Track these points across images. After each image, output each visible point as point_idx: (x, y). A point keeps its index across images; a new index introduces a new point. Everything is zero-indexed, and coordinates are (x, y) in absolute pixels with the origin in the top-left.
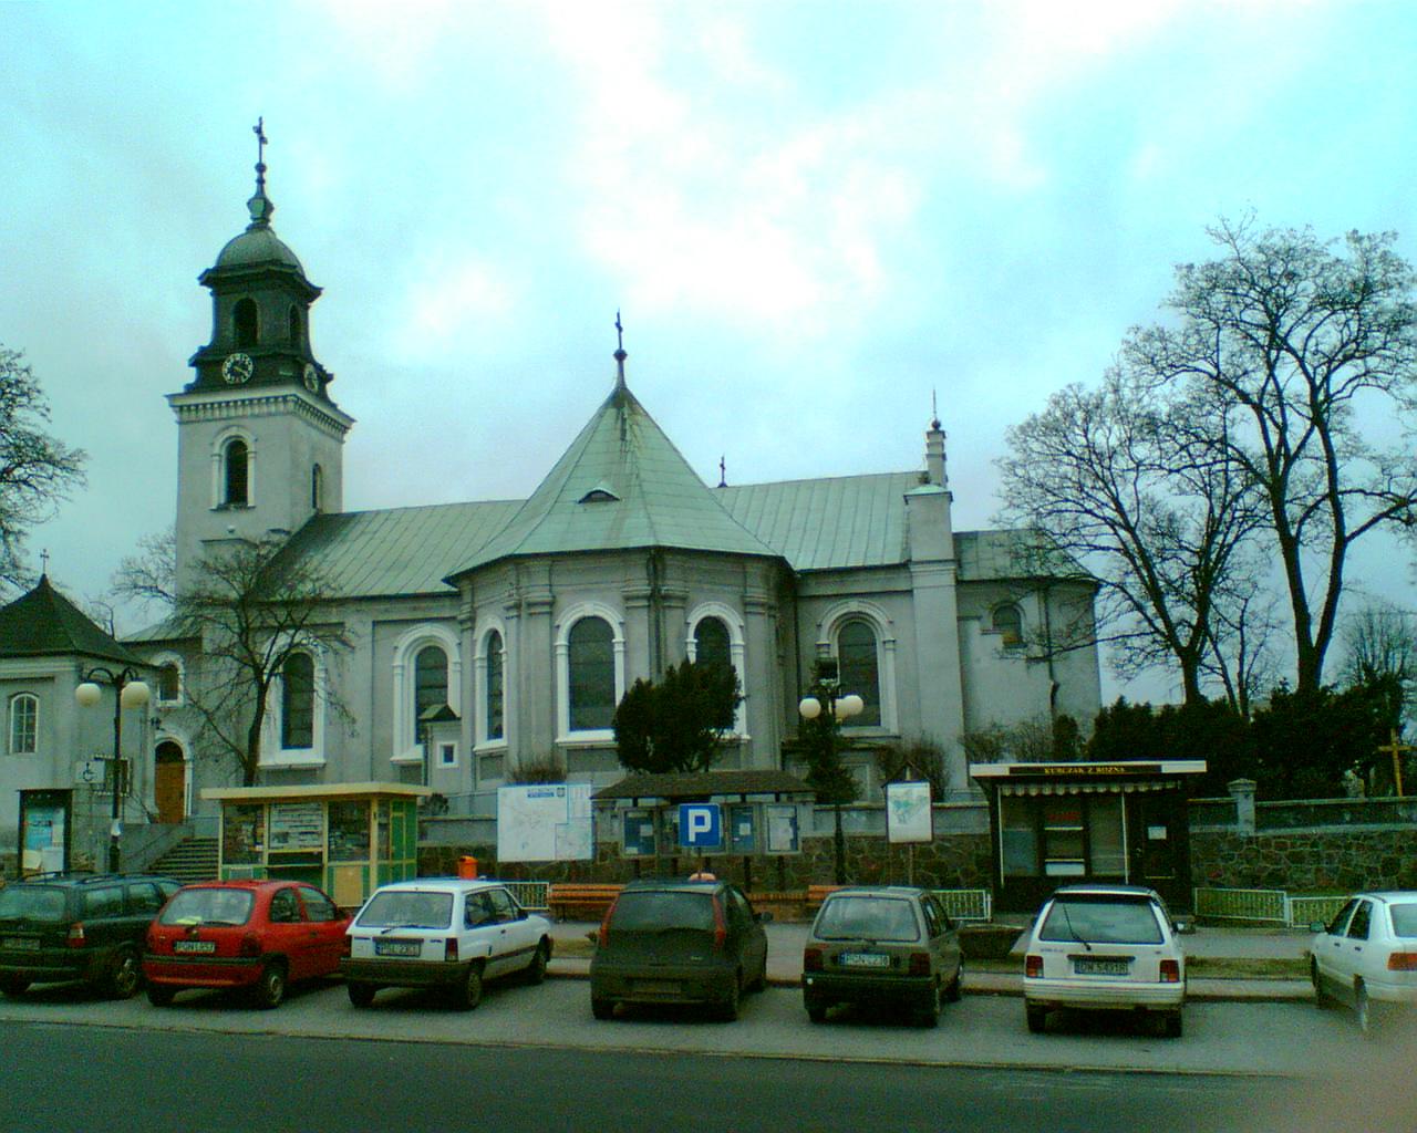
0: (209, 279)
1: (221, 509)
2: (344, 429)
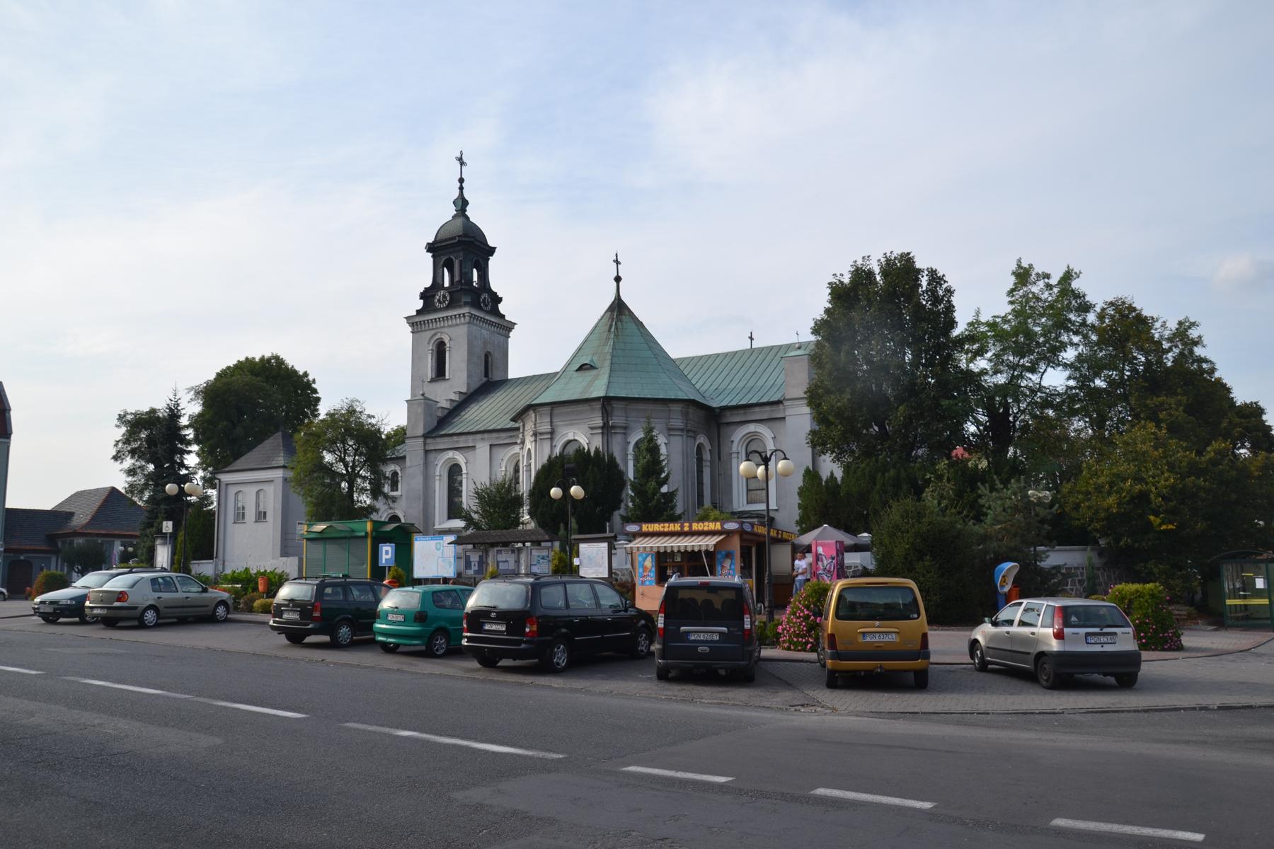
0: (431, 248)
1: (432, 381)
2: (510, 329)
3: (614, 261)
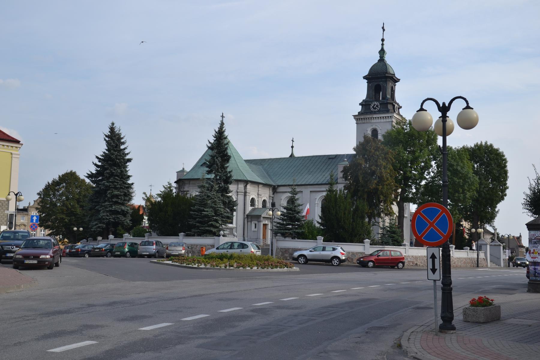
3: (294, 141)
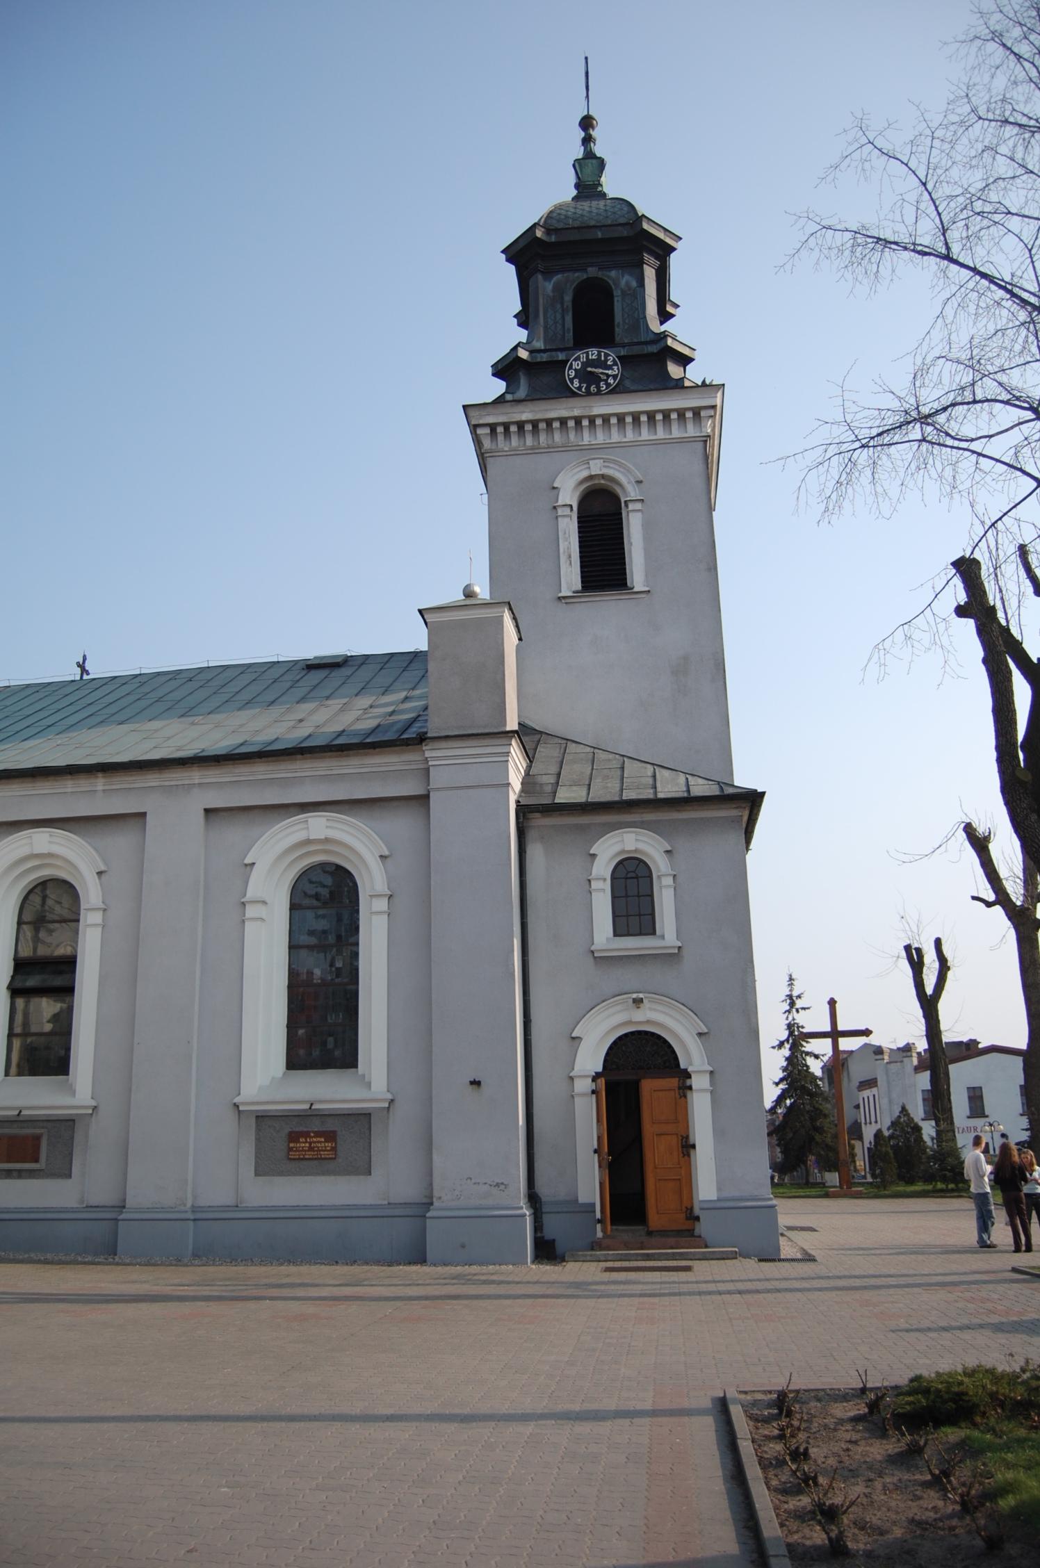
3: (79, 665)
